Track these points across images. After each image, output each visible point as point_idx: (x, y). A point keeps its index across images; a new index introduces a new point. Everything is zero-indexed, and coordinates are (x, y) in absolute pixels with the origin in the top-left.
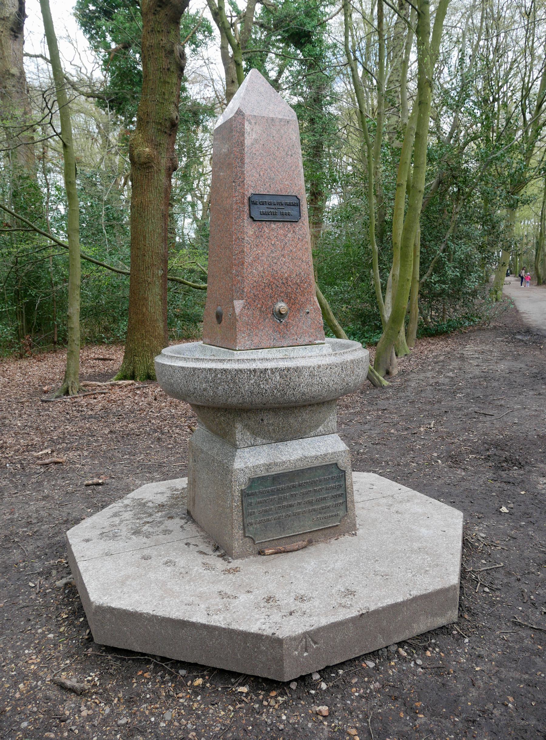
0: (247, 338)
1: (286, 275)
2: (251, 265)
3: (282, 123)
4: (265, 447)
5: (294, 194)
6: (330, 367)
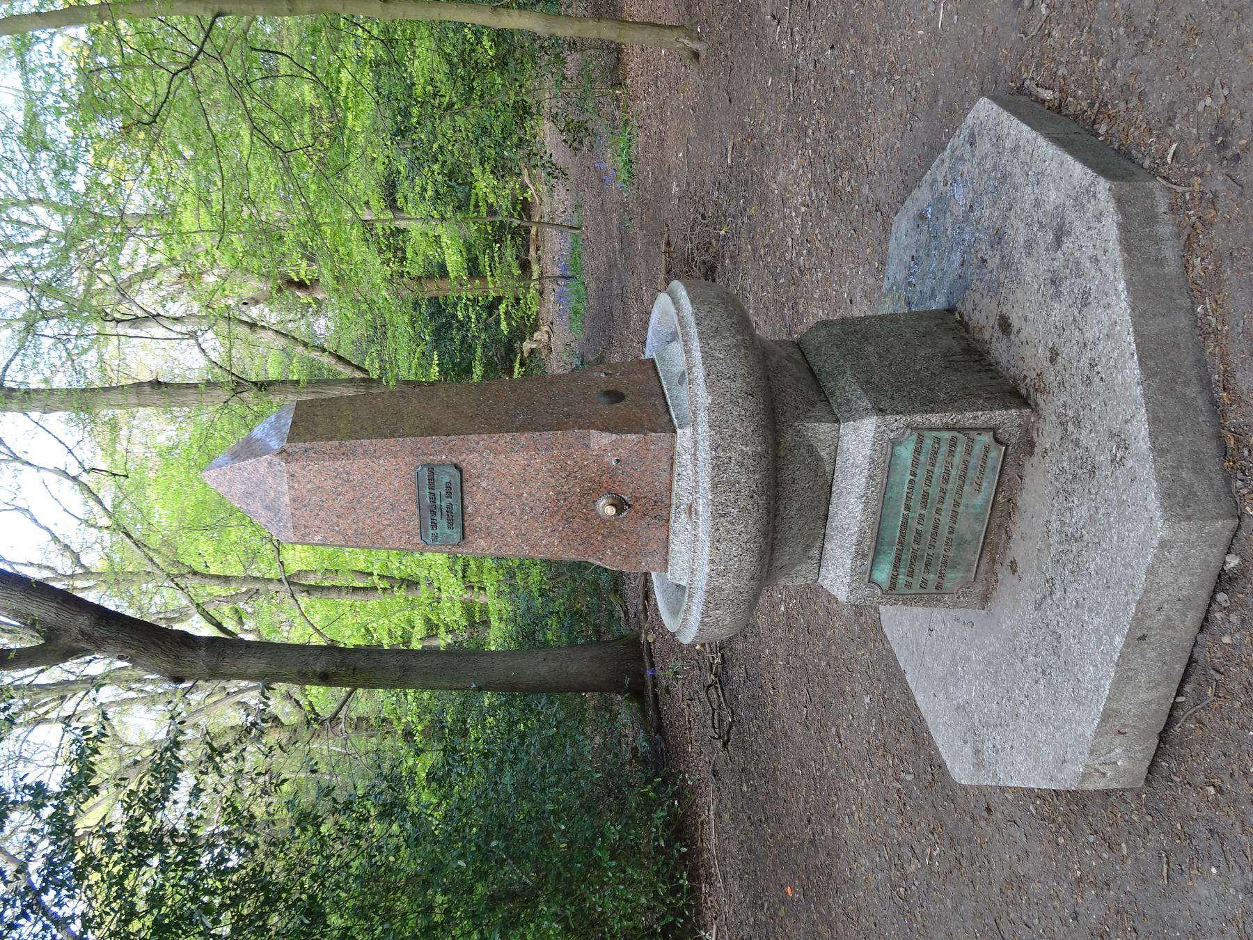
1: (551, 493)
2: (533, 546)
3: (296, 485)
4: (828, 546)
6: (716, 542)
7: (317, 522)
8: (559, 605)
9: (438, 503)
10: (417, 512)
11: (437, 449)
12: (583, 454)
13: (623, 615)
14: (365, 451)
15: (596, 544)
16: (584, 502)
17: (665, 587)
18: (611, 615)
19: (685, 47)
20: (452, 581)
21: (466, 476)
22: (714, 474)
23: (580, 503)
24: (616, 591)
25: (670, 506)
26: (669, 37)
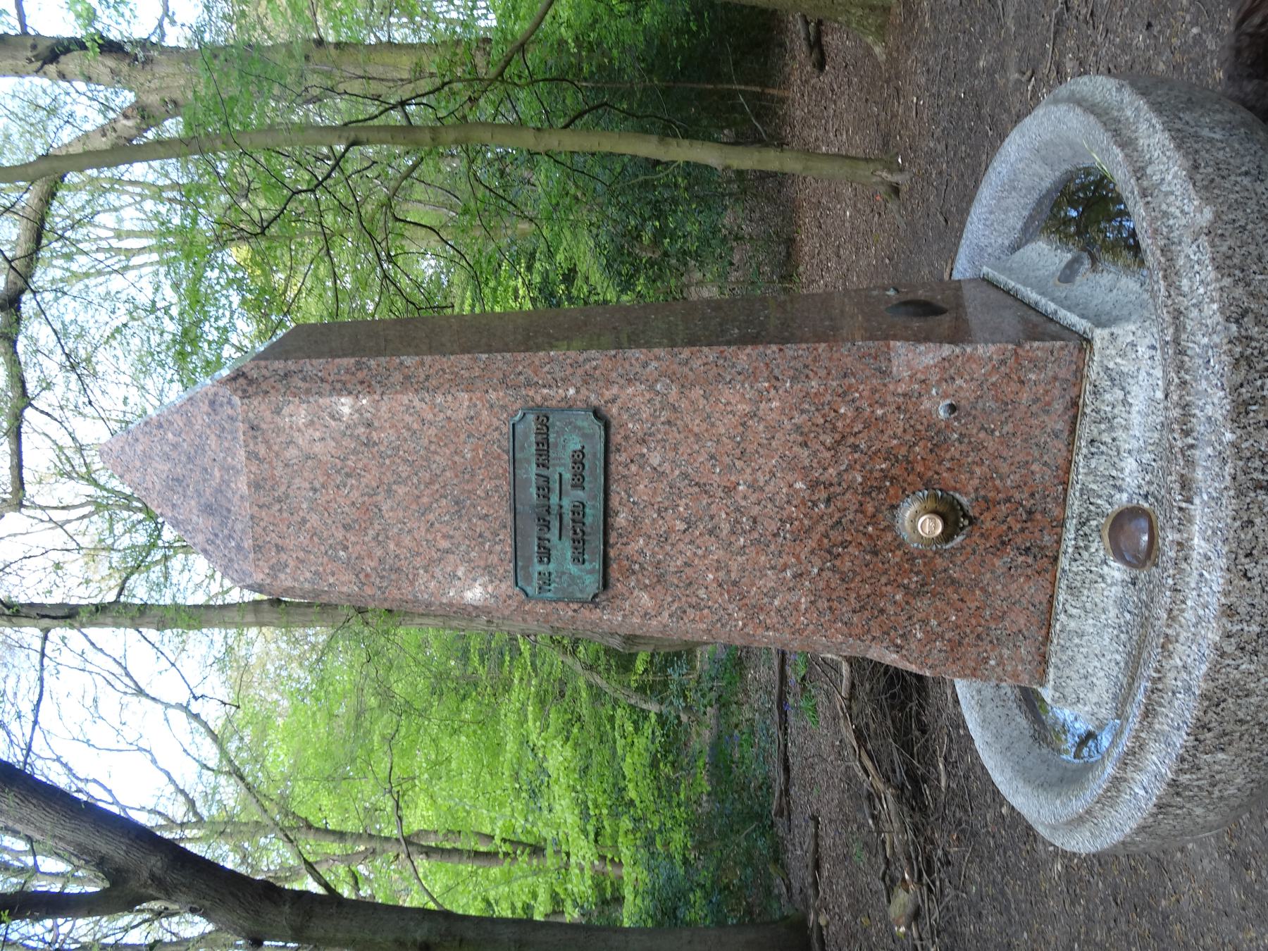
0: (1006, 652)
2: (754, 611)
3: (262, 450)
5: (506, 429)
7: (303, 539)
8: (704, 876)
9: (554, 499)
10: (510, 523)
11: (559, 375)
12: (874, 391)
13: (784, 890)
14: (407, 378)
15: (891, 610)
16: (870, 509)
17: (1005, 741)
18: (768, 891)
19: (883, 182)
20: (583, 843)
21: (617, 439)
22: (1238, 379)
23: (861, 509)
24: (776, 860)
25: (1062, 524)
26: (864, 171)
